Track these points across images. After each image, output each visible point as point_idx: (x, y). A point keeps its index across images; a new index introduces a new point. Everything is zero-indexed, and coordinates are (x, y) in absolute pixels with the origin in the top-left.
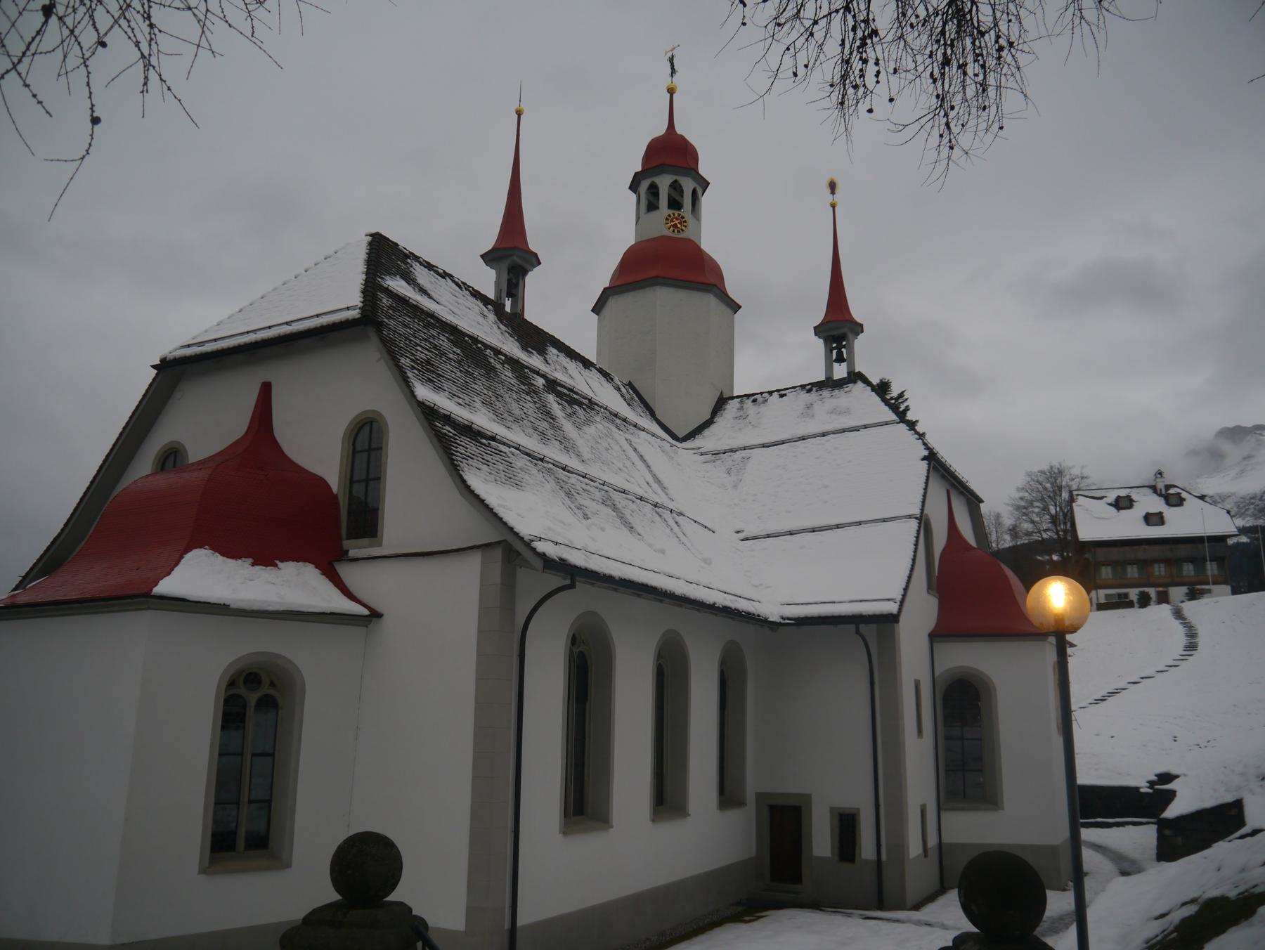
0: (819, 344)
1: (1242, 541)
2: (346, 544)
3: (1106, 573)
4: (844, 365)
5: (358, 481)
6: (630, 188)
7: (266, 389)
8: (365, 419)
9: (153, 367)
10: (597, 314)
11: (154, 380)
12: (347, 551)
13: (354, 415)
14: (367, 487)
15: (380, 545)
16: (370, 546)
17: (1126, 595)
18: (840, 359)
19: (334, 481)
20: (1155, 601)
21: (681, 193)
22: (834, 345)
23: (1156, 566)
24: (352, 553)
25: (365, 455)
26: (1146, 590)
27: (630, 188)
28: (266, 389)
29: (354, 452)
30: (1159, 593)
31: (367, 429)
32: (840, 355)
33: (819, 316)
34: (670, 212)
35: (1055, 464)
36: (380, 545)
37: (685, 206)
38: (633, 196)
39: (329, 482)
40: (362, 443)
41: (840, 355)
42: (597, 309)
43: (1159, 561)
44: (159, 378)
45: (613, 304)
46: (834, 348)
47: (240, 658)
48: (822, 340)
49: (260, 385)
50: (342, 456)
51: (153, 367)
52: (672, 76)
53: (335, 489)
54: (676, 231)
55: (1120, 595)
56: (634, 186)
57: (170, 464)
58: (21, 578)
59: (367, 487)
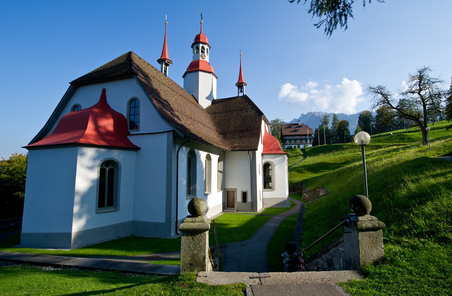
0: (237, 87)
1: (66, 251)
2: (129, 131)
3: (288, 141)
4: (242, 93)
5: (132, 115)
6: (191, 47)
7: (104, 91)
8: (72, 107)
9: (70, 83)
10: (184, 78)
11: (70, 87)
12: (130, 133)
13: (130, 98)
14: (134, 116)
15: (139, 131)
16: (136, 131)
17: (291, 146)
18: (241, 92)
19: (125, 115)
20: (380, 107)
21: (204, 49)
22: (240, 88)
23: (298, 140)
24: (131, 133)
25: (134, 108)
26: (295, 145)
27: (191, 47)
28: (104, 91)
29: (130, 107)
30: (298, 146)
31: (134, 102)
32: (241, 90)
33: (237, 82)
34: (202, 53)
35: (277, 118)
36: (139, 131)
37: (205, 52)
38: (192, 49)
39: (123, 115)
40: (132, 105)
41: (241, 90)
42: (184, 77)
43: (298, 139)
44: (72, 86)
45: (188, 75)
46: (240, 89)
47: (108, 158)
48: (237, 87)
49: (102, 89)
50: (127, 109)
51: (70, 83)
52: (202, 19)
53: (126, 117)
54: (202, 58)
55: (290, 146)
56: (192, 47)
57: (76, 109)
58: (32, 140)
59: (134, 116)
